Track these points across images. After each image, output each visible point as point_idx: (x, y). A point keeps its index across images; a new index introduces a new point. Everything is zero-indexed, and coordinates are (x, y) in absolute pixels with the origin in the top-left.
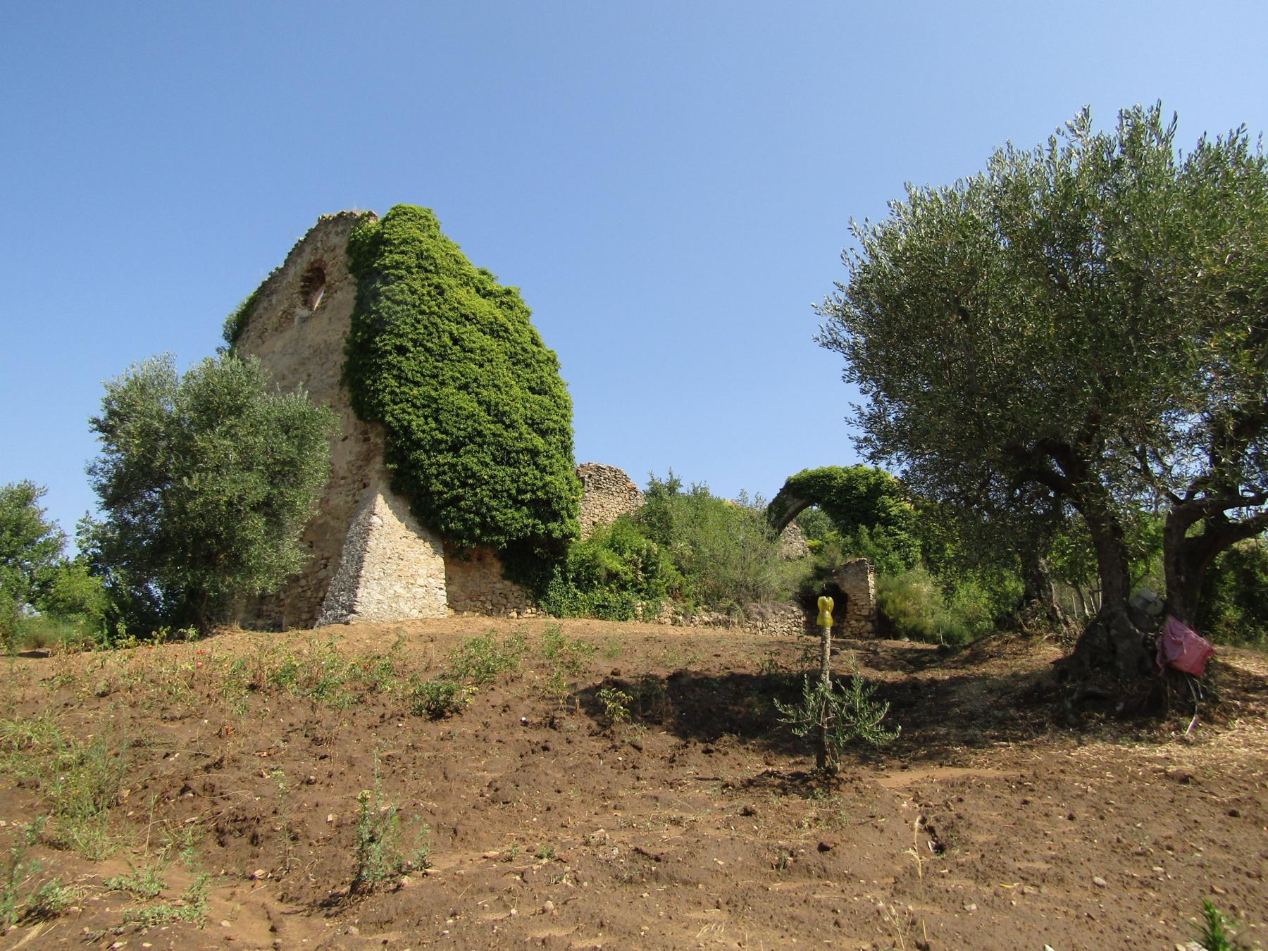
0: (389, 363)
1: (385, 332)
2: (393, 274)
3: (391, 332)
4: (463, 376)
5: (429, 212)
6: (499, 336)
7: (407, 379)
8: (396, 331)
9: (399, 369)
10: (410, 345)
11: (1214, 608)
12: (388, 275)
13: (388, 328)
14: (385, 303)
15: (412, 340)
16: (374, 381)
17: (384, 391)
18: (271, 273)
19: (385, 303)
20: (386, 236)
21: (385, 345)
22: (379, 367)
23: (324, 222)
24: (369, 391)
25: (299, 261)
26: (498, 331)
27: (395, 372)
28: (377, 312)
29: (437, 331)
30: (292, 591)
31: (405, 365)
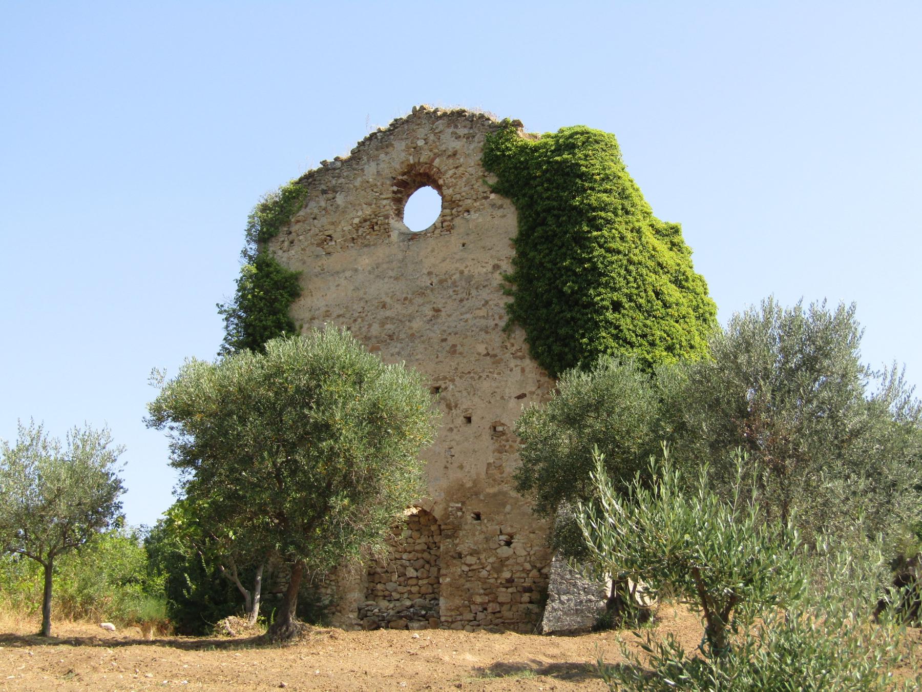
0: (607, 321)
1: (599, 285)
2: (601, 218)
3: (606, 285)
4: (668, 336)
5: (614, 136)
6: (683, 287)
7: (625, 340)
8: (612, 285)
9: (617, 327)
10: (624, 300)
11: (116, 500)
12: (595, 218)
13: (604, 280)
14: (598, 252)
15: (626, 295)
16: (591, 340)
17: (605, 352)
18: (324, 163)
19: (598, 252)
20: (584, 169)
21: (602, 300)
22: (596, 325)
23: (419, 115)
24: (582, 351)
25: (382, 156)
26: (681, 281)
27: (614, 332)
28: (590, 260)
29: (644, 285)
30: (453, 569)
31: (622, 322)
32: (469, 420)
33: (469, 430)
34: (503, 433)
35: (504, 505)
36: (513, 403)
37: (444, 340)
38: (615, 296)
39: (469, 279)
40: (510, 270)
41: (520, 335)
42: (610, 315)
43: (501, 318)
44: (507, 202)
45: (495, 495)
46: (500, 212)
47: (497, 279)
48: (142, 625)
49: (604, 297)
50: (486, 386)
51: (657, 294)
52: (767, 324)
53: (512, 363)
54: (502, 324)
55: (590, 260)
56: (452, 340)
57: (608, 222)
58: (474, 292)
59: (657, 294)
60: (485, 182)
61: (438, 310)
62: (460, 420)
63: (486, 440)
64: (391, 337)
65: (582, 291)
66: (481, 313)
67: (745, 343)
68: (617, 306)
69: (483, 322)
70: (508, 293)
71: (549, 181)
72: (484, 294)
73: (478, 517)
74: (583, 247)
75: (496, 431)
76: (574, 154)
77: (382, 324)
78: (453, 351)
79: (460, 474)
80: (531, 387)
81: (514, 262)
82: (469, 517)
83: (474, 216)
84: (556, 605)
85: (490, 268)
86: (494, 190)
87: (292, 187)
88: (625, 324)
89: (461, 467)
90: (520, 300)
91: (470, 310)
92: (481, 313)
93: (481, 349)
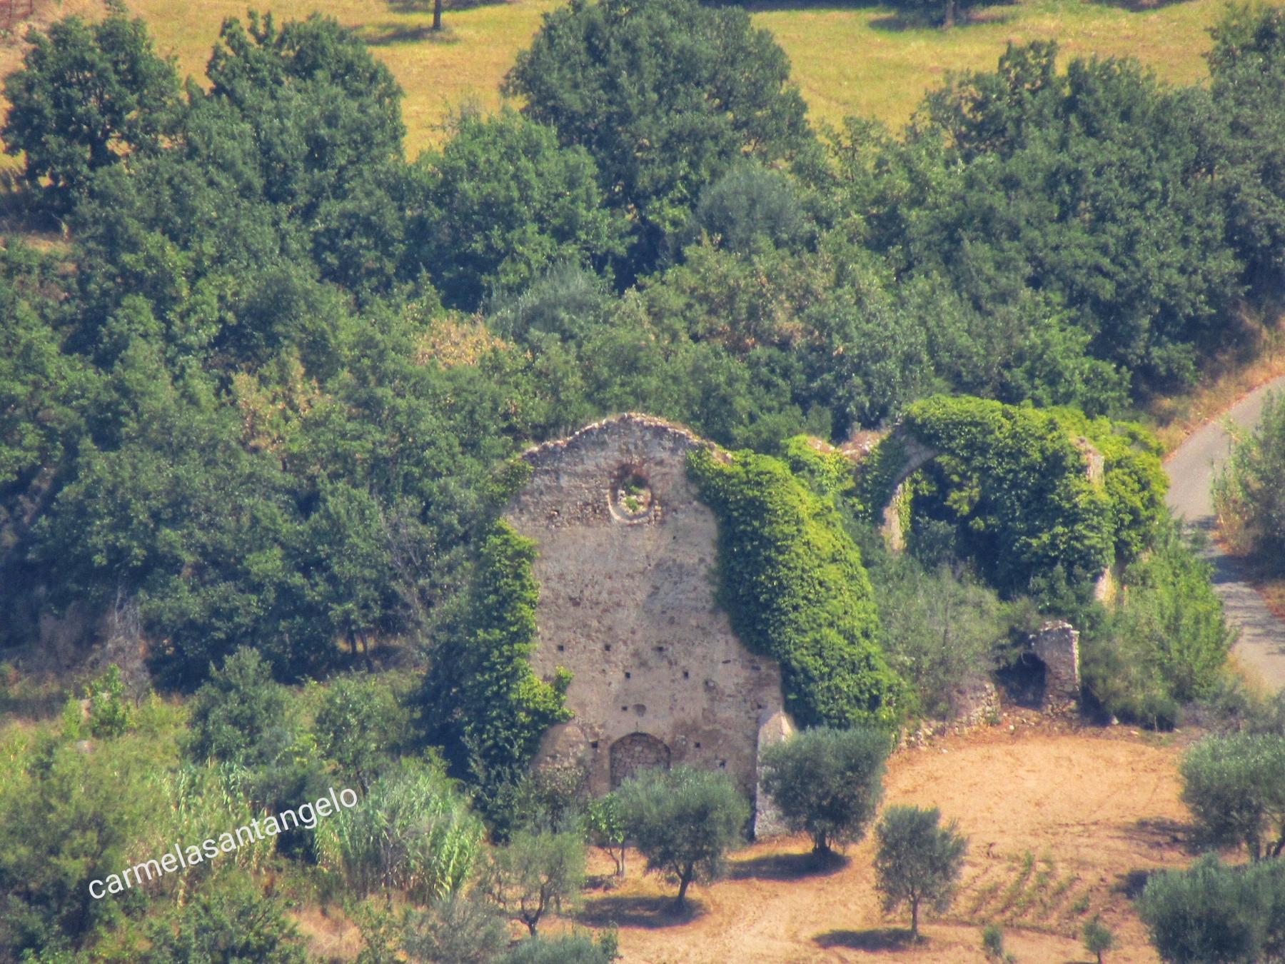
16: (780, 634)
32: (686, 675)
33: (687, 683)
34: (714, 688)
35: (717, 740)
36: (721, 666)
37: (664, 612)
38: (795, 601)
39: (681, 567)
40: (714, 565)
41: (723, 619)
42: (792, 616)
43: (707, 602)
44: (708, 510)
45: (710, 732)
46: (702, 518)
47: (703, 570)
48: (49, 752)
49: (784, 602)
50: (699, 651)
51: (821, 584)
52: (1078, 727)
53: (719, 636)
54: (709, 606)
55: (777, 578)
56: (670, 613)
57: (788, 547)
58: (685, 578)
59: (821, 584)
60: (688, 491)
61: (657, 588)
62: (679, 675)
63: (701, 694)
64: (618, 605)
65: (772, 600)
66: (692, 595)
67: (1199, 814)
68: (796, 608)
69: (693, 603)
70: (712, 583)
71: (744, 508)
72: (694, 581)
73: (698, 745)
74: (773, 567)
75: (708, 686)
76: (762, 492)
77: (610, 593)
78: (672, 621)
79: (682, 715)
80: (733, 656)
81: (716, 559)
82: (692, 745)
83: (681, 516)
84: (763, 816)
85: (696, 560)
86: (696, 498)
87: (1191, 821)
88: (802, 618)
89: (683, 709)
90: (1187, 790)
91: (683, 592)
92: (692, 595)
93: (694, 622)
